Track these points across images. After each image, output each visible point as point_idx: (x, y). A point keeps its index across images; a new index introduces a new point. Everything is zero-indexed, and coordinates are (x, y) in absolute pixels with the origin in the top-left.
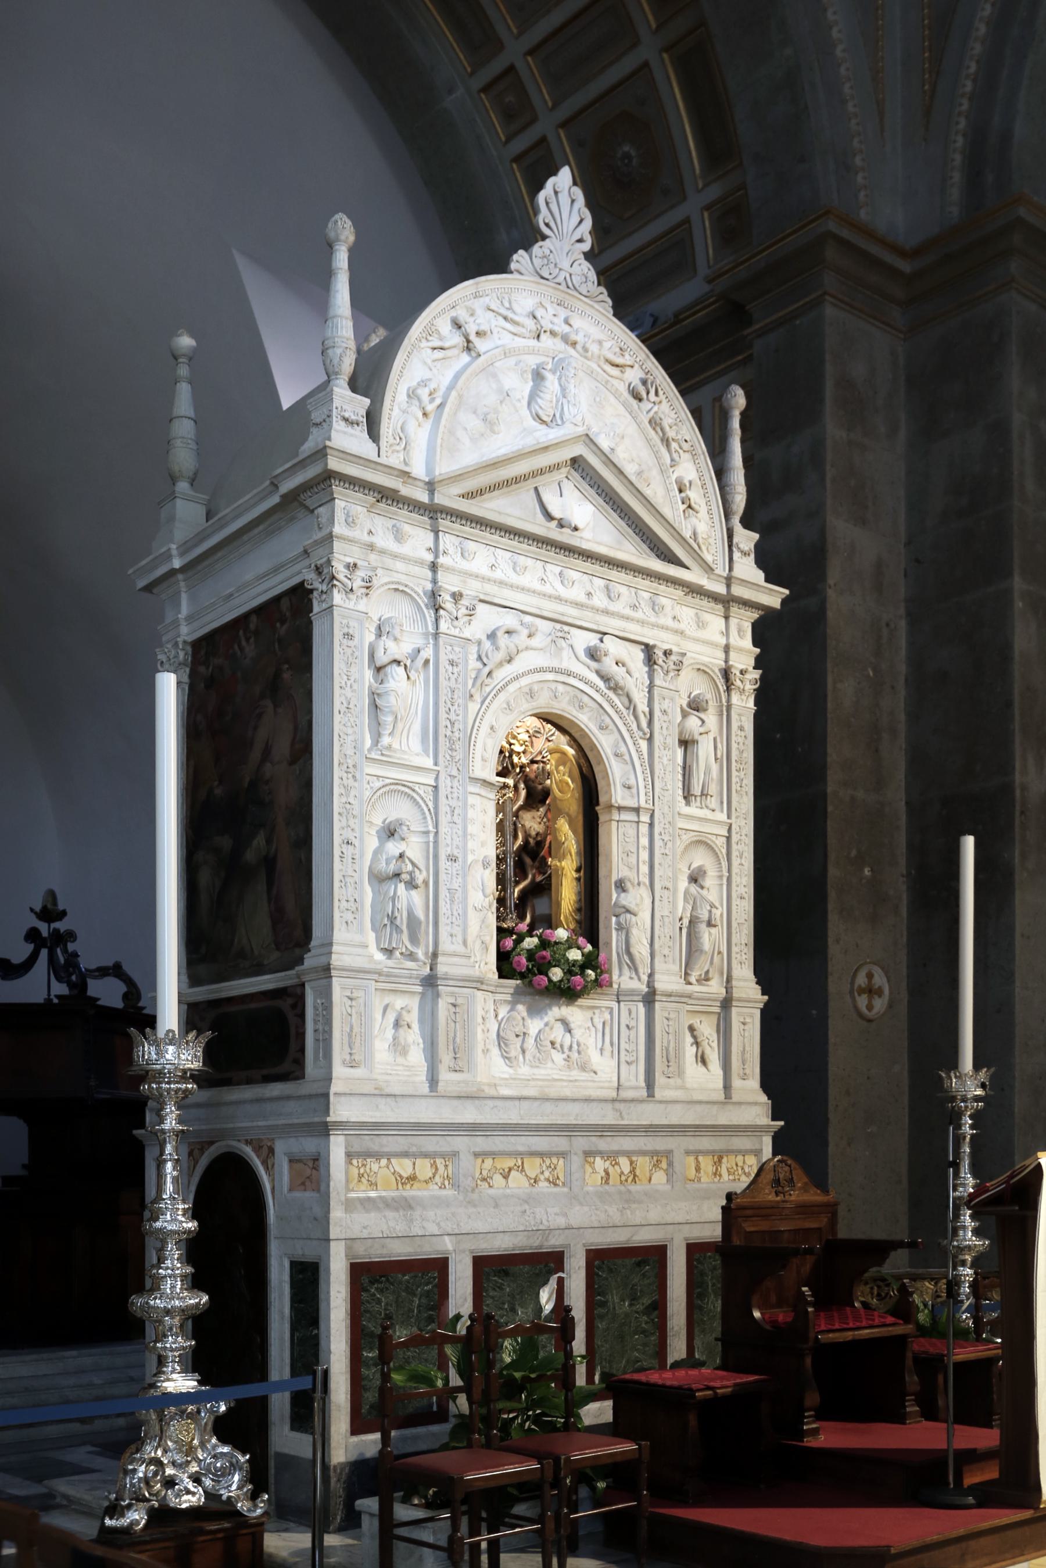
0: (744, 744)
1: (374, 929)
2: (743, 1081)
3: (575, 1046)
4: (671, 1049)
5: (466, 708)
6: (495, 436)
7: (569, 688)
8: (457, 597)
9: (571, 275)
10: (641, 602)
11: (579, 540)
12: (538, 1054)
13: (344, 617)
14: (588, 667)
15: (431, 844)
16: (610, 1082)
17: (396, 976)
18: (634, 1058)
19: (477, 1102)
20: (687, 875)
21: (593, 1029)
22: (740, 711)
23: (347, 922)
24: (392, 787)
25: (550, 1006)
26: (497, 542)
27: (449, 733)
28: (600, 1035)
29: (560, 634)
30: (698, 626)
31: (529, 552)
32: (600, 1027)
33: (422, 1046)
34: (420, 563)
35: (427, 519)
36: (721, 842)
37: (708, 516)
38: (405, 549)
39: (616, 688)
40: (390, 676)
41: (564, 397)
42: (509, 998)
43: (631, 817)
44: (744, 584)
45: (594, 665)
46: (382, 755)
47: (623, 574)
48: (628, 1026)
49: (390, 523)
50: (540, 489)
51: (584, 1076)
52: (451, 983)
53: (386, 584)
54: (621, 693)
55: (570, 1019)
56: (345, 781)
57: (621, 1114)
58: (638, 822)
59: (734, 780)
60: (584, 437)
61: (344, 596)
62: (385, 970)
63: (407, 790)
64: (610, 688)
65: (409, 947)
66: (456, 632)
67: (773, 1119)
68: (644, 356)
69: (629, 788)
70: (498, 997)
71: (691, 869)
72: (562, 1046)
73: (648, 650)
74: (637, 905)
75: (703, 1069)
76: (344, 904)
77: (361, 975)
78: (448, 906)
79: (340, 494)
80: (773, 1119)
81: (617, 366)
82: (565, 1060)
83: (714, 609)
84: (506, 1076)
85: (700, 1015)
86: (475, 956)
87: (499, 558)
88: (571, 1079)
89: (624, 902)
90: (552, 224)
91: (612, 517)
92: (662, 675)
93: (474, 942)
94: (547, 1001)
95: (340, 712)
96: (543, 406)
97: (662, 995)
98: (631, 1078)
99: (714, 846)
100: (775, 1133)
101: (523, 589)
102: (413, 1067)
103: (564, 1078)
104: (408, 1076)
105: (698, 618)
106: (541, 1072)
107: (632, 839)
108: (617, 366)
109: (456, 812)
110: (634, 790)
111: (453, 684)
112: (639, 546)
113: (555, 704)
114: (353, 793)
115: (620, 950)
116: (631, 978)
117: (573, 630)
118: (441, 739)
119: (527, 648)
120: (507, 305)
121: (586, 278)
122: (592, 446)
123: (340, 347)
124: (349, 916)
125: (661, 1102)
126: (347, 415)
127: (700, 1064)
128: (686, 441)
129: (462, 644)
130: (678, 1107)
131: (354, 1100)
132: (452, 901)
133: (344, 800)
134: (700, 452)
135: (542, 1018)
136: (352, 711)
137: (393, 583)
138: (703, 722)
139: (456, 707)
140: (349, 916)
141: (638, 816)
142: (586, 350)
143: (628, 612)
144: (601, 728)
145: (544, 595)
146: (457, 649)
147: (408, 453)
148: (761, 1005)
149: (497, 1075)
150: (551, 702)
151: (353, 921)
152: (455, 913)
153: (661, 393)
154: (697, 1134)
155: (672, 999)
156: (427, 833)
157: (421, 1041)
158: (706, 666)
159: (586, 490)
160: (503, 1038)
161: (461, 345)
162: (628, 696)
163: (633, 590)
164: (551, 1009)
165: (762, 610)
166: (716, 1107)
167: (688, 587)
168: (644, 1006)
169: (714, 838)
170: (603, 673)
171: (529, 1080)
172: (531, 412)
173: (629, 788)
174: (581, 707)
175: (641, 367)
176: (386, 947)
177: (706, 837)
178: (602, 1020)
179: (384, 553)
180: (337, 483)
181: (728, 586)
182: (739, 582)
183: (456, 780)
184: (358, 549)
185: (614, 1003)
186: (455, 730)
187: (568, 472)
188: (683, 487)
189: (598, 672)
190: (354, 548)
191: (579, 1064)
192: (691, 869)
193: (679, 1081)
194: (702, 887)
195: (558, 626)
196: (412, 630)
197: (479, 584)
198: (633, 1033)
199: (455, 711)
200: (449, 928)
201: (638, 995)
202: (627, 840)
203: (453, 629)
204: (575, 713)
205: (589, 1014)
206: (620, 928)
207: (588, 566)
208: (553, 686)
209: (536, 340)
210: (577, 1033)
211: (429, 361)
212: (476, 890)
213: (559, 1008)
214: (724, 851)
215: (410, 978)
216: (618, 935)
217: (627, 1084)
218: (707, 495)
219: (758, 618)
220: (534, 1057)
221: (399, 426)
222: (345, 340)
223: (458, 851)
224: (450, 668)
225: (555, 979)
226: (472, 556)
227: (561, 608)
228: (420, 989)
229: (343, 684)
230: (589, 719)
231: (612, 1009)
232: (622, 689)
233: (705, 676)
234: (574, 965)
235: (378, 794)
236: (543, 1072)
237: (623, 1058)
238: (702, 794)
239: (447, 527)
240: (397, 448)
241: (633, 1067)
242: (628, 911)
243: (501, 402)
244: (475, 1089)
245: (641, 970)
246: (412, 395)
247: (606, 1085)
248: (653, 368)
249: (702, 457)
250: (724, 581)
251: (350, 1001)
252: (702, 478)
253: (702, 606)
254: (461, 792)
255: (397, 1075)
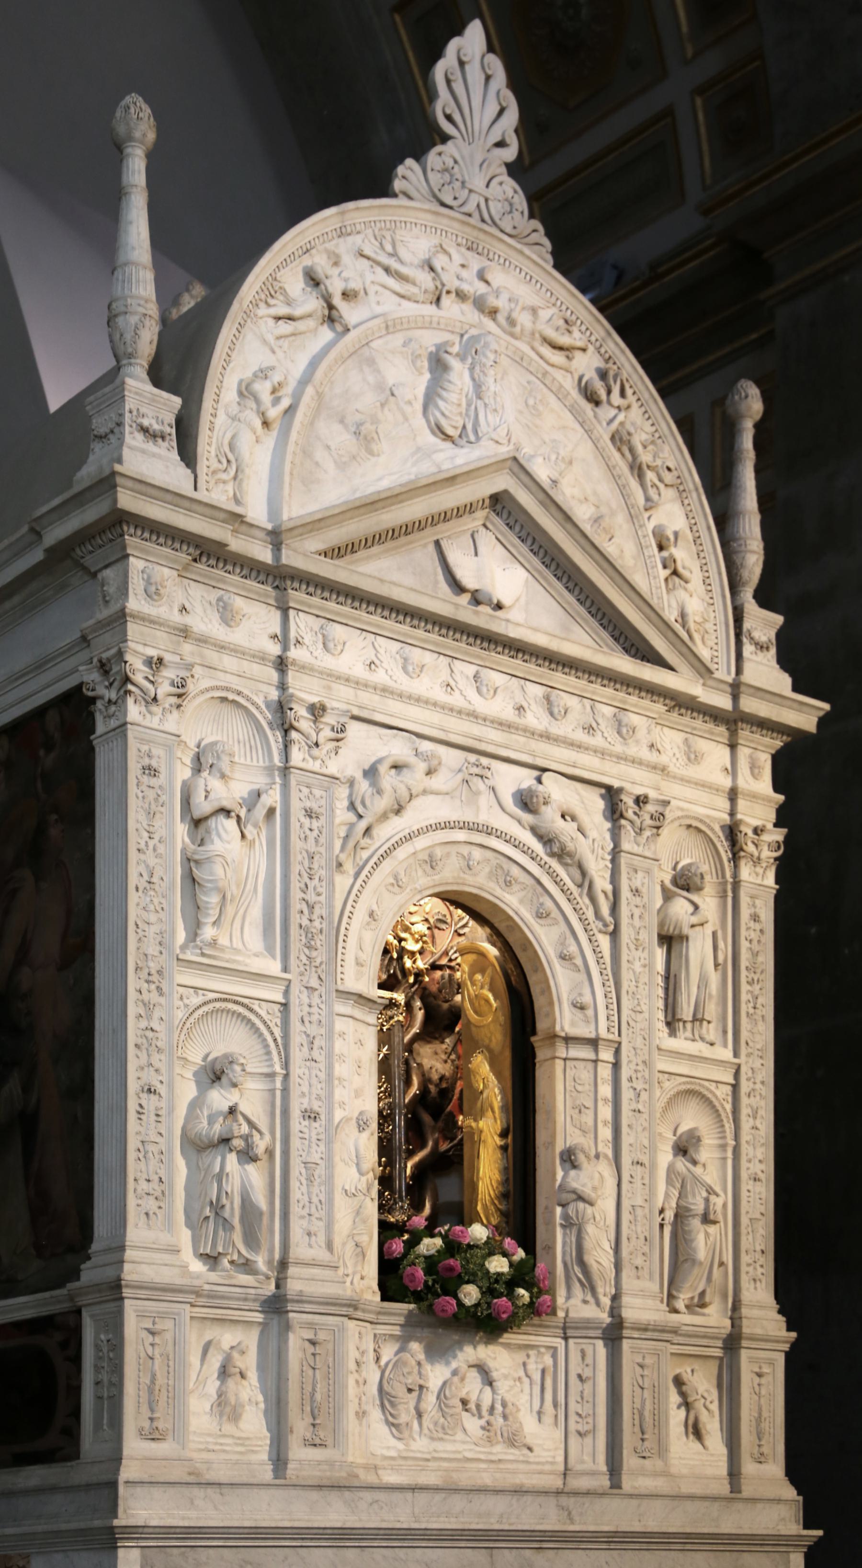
0: (759, 941)
1: (189, 1224)
2: (758, 1465)
3: (499, 1408)
4: (647, 1414)
5: (331, 884)
6: (373, 460)
7: (489, 854)
8: (317, 711)
9: (487, 200)
10: (600, 721)
11: (504, 623)
12: (442, 1420)
13: (142, 741)
14: (519, 822)
15: (278, 1094)
16: (552, 1463)
17: (223, 1297)
18: (589, 1427)
19: (347, 1494)
20: (671, 1143)
21: (526, 1381)
22: (754, 892)
23: (147, 1214)
24: (218, 1005)
25: (460, 1345)
26: (378, 626)
27: (305, 922)
28: (537, 1389)
29: (475, 770)
30: (689, 759)
31: (425, 641)
32: (537, 1377)
33: (262, 1406)
34: (260, 657)
35: (269, 589)
36: (723, 1093)
37: (703, 587)
38: (238, 636)
39: (562, 854)
40: (214, 833)
41: (479, 397)
42: (397, 1330)
43: (586, 1053)
44: (760, 694)
45: (527, 818)
46: (203, 955)
47: (573, 679)
48: (580, 1376)
49: (214, 595)
50: (442, 543)
51: (514, 1454)
52: (308, 1307)
53: (207, 690)
54: (569, 861)
55: (491, 1364)
56: (146, 996)
57: (569, 1514)
58: (595, 1061)
59: (744, 997)
60: (509, 463)
61: (143, 709)
62: (206, 1287)
63: (240, 1009)
64: (552, 855)
65: (244, 1251)
66: (316, 766)
67: (806, 1526)
68: (603, 333)
69: (582, 1008)
70: (381, 1330)
71: (679, 1132)
72: (478, 1407)
73: (611, 795)
74: (594, 1189)
75: (697, 1446)
76: (143, 1186)
77: (169, 1296)
78: (304, 1189)
79: (136, 548)
80: (806, 1526)
81: (561, 348)
82: (483, 1428)
83: (712, 733)
84: (393, 1453)
85: (691, 1360)
86: (345, 1265)
87: (382, 651)
88: (493, 1458)
89: (574, 1185)
90: (457, 117)
91: (554, 588)
92: (633, 834)
93: (344, 1244)
94: (456, 1337)
95: (137, 889)
96: (447, 413)
97: (633, 1329)
98: (585, 1458)
99: (713, 1099)
100: (810, 1548)
101: (572, 744)
102: (248, 1439)
103: (482, 1457)
104: (241, 1453)
105: (689, 747)
106: (446, 1448)
107: (587, 1087)
108: (561, 348)
109: (317, 1043)
110: (590, 1012)
111: (311, 846)
112: (597, 634)
113: (469, 878)
114: (157, 1014)
115: (568, 1259)
116: (585, 1302)
117: (496, 765)
118: (294, 931)
119: (425, 792)
120: (389, 248)
121: (511, 205)
122: (523, 476)
123: (135, 313)
124: (151, 1204)
125: (631, 1496)
126: (146, 422)
127: (691, 1437)
128: (669, 469)
129: (326, 784)
130: (658, 1504)
131: (157, 1492)
132: (310, 1180)
133: (143, 1024)
134: (691, 486)
135: (448, 1363)
136: (157, 887)
137: (217, 688)
138: (696, 907)
139: (316, 881)
140: (151, 1204)
141: (596, 1051)
142: (512, 322)
143: (580, 736)
144: (539, 916)
145: (451, 710)
146: (317, 792)
147: (240, 484)
148: (786, 1347)
149: (379, 1452)
150: (462, 875)
151: (158, 1211)
152: (315, 1200)
153: (629, 392)
154: (688, 1547)
155: (649, 1335)
156: (271, 1076)
157: (261, 1398)
158: (701, 821)
159: (514, 546)
160: (388, 1394)
161: (320, 313)
162: (581, 867)
163: (587, 703)
164: (461, 1349)
165: (788, 735)
166: (716, 1505)
167: (672, 699)
168: (606, 1345)
169: (712, 1087)
170: (542, 831)
171: (428, 1460)
172: (428, 421)
173: (582, 1008)
174: (508, 884)
175: (598, 350)
176: (208, 1251)
177: (700, 1085)
178: (541, 1367)
179: (205, 642)
180: (132, 531)
181: (735, 697)
182: (752, 691)
183: (316, 993)
184: (165, 635)
185: (559, 1340)
186: (315, 917)
187: (487, 518)
188: (664, 543)
189: (534, 830)
190: (158, 633)
191: (505, 1435)
192: (679, 1132)
193: (659, 1464)
194: (695, 1163)
195: (473, 758)
196: (249, 762)
197: (351, 691)
198: (588, 1387)
199: (315, 888)
200: (304, 1223)
201: (597, 1328)
202: (579, 1088)
203: (311, 760)
204: (498, 892)
205: (520, 1357)
206: (568, 1223)
207: (517, 664)
208: (465, 850)
209: (434, 306)
210: (503, 1386)
211: (271, 339)
212: (347, 1164)
213: (475, 1347)
214: (729, 1107)
215: (245, 1299)
216: (565, 1235)
217: (579, 1467)
218: (702, 555)
219: (782, 748)
220: (436, 1424)
221: (226, 442)
222: (142, 302)
223: (320, 1103)
224: (306, 822)
225: (468, 1302)
226: (339, 648)
227: (476, 730)
228: (259, 1317)
229: (142, 846)
230: (521, 901)
231: (555, 1349)
232: (570, 855)
233: (700, 838)
234: (497, 1281)
235: (196, 1015)
236: (449, 1447)
237: (572, 1426)
238: (695, 1019)
239: (302, 603)
240: (224, 476)
241: (588, 1440)
242: (580, 1198)
243: (383, 405)
244: (344, 1474)
245: (600, 1290)
246: (246, 392)
247: (547, 1467)
248: (617, 352)
249: (694, 495)
250: (729, 689)
251: (151, 1337)
252: (695, 528)
253: (695, 729)
254: (323, 1013)
255: (224, 1451)
